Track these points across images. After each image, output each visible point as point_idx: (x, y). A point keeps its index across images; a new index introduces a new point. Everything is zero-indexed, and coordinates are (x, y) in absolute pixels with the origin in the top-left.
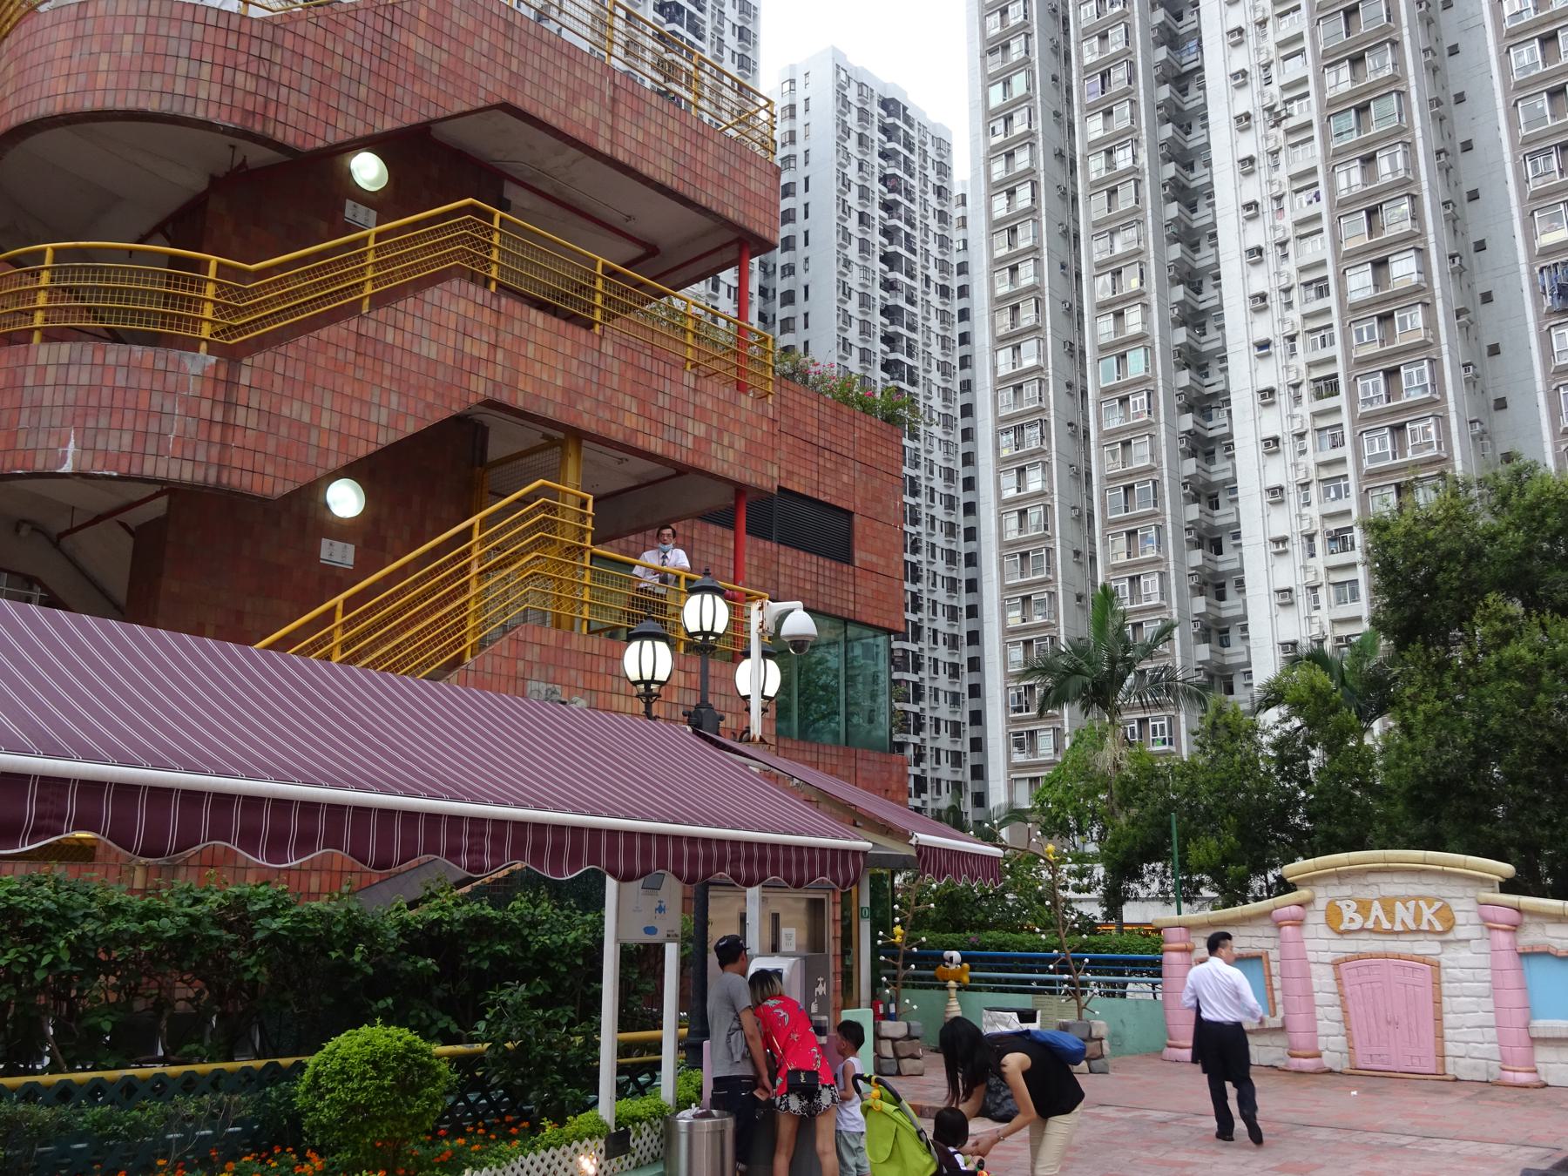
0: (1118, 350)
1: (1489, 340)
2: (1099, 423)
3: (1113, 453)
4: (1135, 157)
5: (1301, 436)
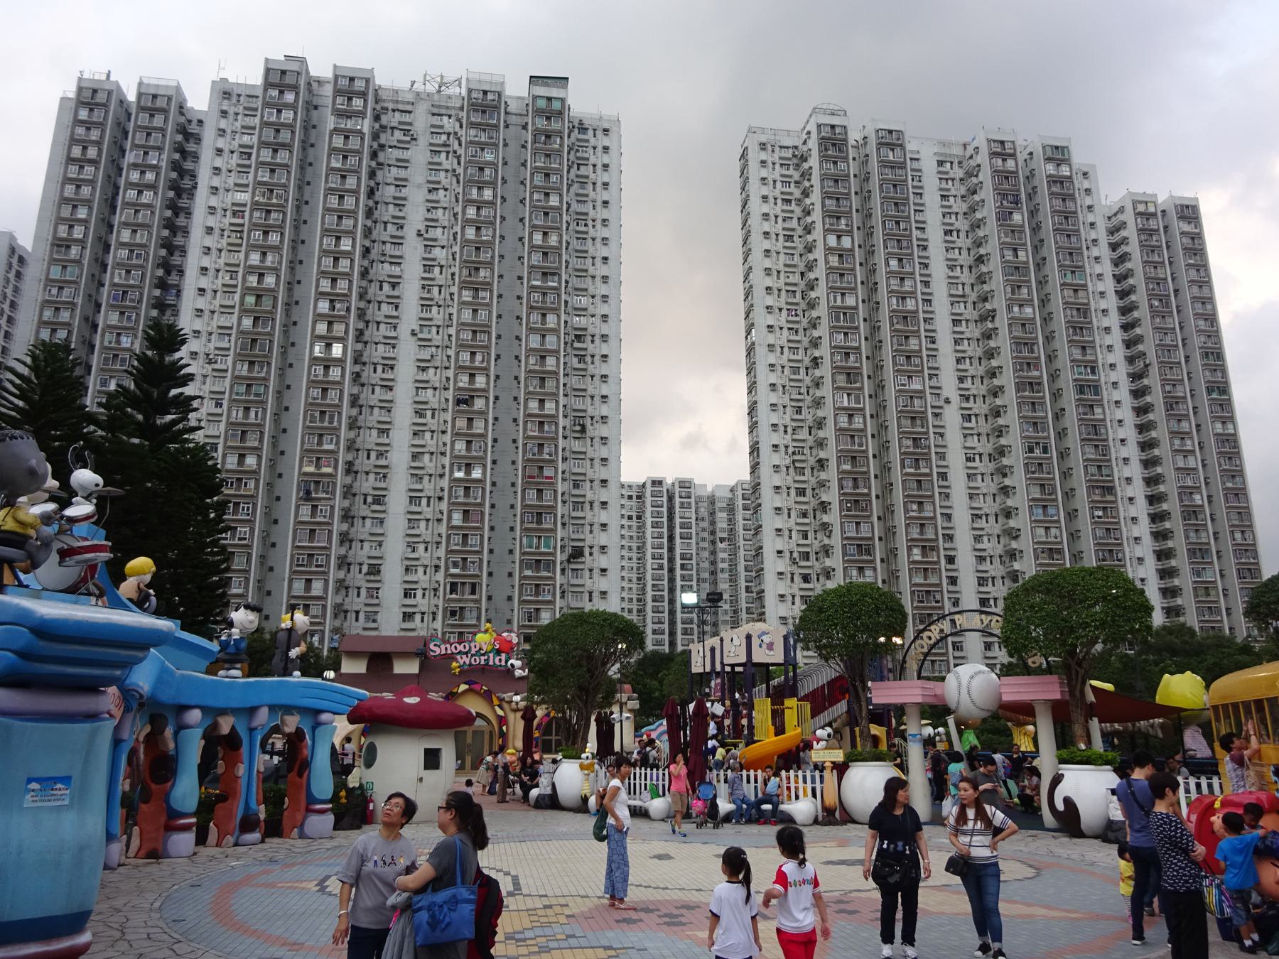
4: (132, 343)
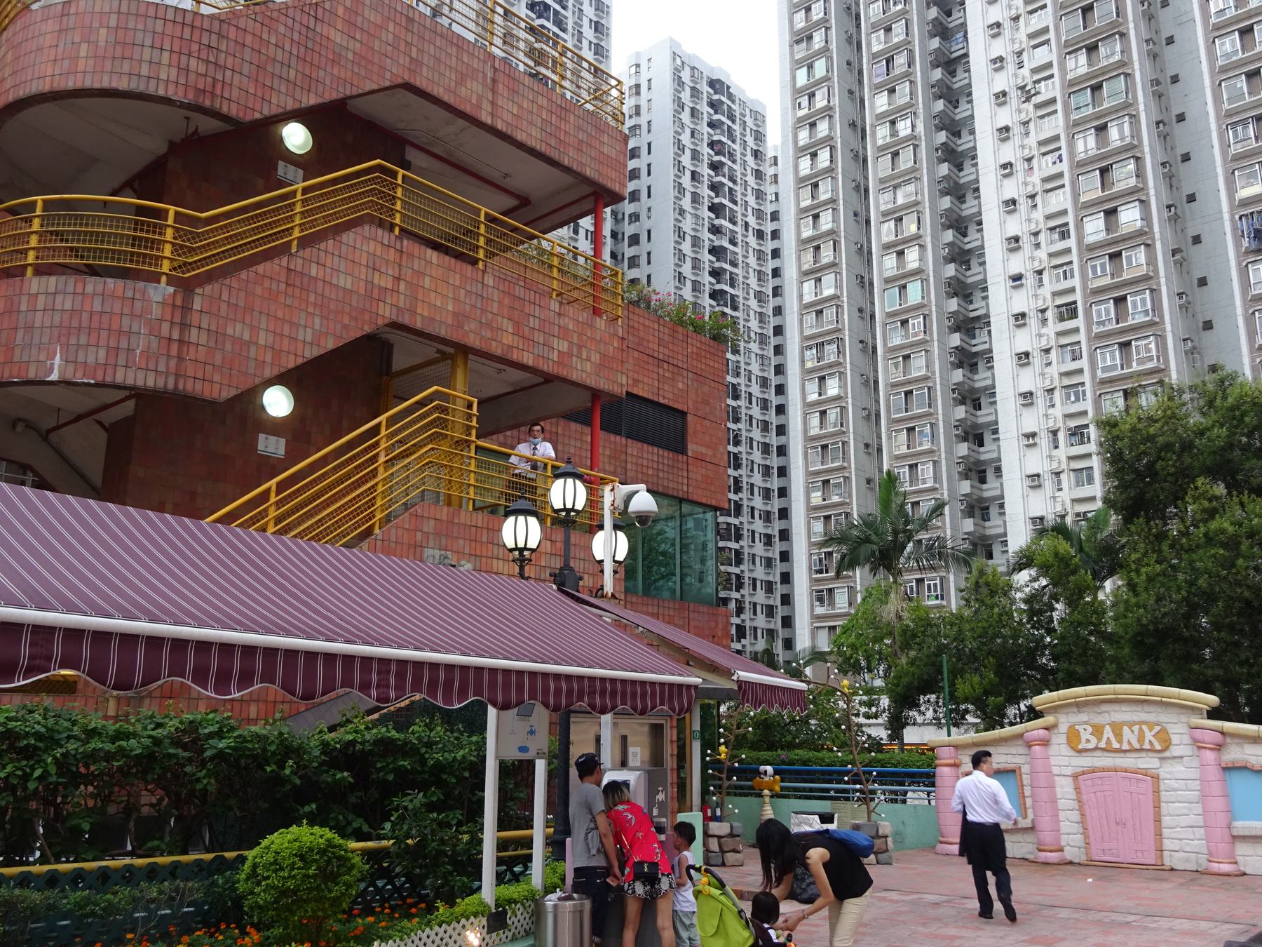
0: (900, 282)
1: (1199, 274)
2: (885, 340)
3: (896, 365)
4: (913, 127)
5: (1047, 351)
